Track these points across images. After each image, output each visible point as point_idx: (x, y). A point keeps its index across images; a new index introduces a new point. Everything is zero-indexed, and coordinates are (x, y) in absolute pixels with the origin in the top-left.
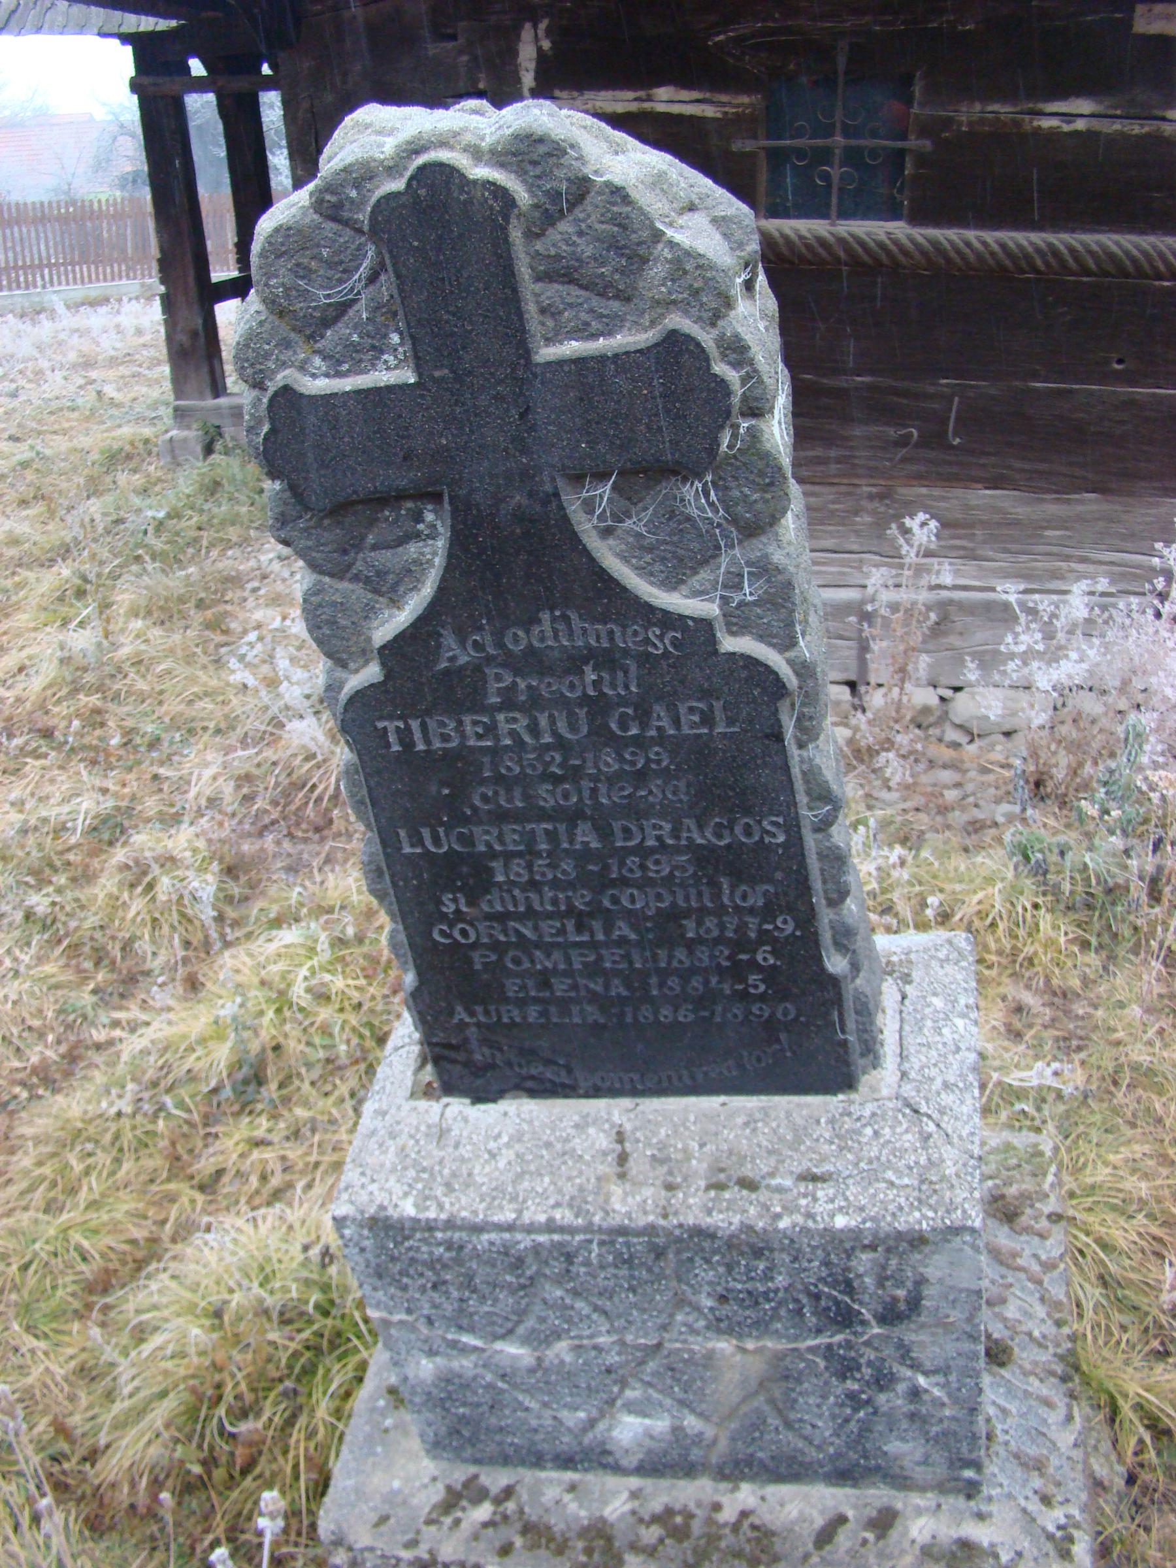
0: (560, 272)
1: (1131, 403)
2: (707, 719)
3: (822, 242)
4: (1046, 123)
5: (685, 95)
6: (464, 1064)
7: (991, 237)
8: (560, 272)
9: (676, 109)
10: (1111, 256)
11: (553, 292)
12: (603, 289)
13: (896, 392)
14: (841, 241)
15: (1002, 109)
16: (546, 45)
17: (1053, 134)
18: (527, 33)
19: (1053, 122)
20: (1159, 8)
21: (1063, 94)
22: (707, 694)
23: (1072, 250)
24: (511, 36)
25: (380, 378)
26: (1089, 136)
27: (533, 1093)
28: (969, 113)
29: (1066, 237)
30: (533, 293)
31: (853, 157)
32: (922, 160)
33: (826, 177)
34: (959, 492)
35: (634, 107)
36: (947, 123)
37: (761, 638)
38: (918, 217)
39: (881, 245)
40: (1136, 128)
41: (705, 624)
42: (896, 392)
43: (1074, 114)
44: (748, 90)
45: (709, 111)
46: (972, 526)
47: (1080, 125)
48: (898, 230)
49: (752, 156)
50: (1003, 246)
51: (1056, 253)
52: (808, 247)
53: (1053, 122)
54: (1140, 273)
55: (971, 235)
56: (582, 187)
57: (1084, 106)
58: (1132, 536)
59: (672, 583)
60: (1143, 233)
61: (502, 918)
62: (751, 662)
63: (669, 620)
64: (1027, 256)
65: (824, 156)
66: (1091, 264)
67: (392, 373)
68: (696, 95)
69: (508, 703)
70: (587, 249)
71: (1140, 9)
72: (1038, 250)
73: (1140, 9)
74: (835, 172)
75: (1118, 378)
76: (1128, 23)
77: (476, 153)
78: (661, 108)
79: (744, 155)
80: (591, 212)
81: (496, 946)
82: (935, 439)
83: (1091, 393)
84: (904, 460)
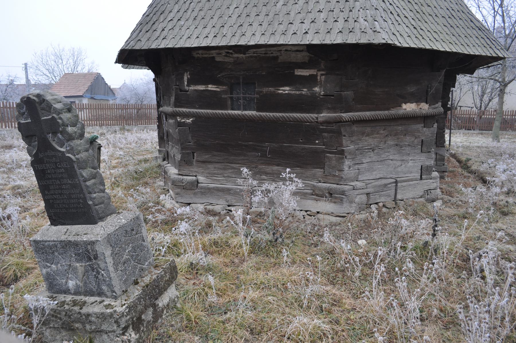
0: (43, 109)
1: (304, 149)
2: (67, 165)
3: (239, 115)
4: (280, 92)
5: (214, 86)
6: (54, 222)
7: (271, 114)
8: (43, 109)
9: (212, 89)
10: (295, 118)
11: (43, 111)
12: (47, 111)
13: (258, 146)
14: (243, 115)
15: (272, 89)
16: (189, 77)
17: (282, 94)
18: (185, 75)
19: (282, 92)
20: (299, 70)
21: (283, 86)
22: (66, 161)
23: (287, 117)
24: (183, 75)
25: (29, 121)
26: (288, 94)
27: (61, 225)
28: (265, 90)
29: (287, 114)
30: (40, 112)
31: (244, 99)
32: (257, 99)
33: (240, 103)
34: (271, 167)
35: (204, 89)
36: (261, 92)
37: (72, 154)
38: (258, 110)
39: (250, 116)
40: (298, 93)
41: (63, 152)
42: (258, 146)
43: (285, 90)
44: (225, 86)
45: (218, 90)
46: (274, 174)
47: (287, 92)
48: (254, 113)
49: (226, 98)
50: (274, 116)
51: (284, 117)
52: (255, 117)
53: (282, 92)
54: (302, 122)
55: (268, 114)
56: (44, 100)
57: (287, 88)
58: (307, 177)
59: (62, 147)
60: (302, 113)
61: (52, 194)
62: (69, 157)
63: (60, 151)
64: (278, 118)
65: (239, 99)
66: (291, 119)
67: (29, 121)
68: (216, 86)
69: (47, 163)
70: (45, 107)
71: (296, 70)
72: (281, 117)
73: (296, 70)
74: (241, 101)
75: (301, 143)
76: (294, 73)
77: (34, 96)
78: (209, 89)
79: (224, 98)
80: (45, 102)
81: (52, 199)
82: (264, 155)
83: (296, 146)
84: (259, 160)
